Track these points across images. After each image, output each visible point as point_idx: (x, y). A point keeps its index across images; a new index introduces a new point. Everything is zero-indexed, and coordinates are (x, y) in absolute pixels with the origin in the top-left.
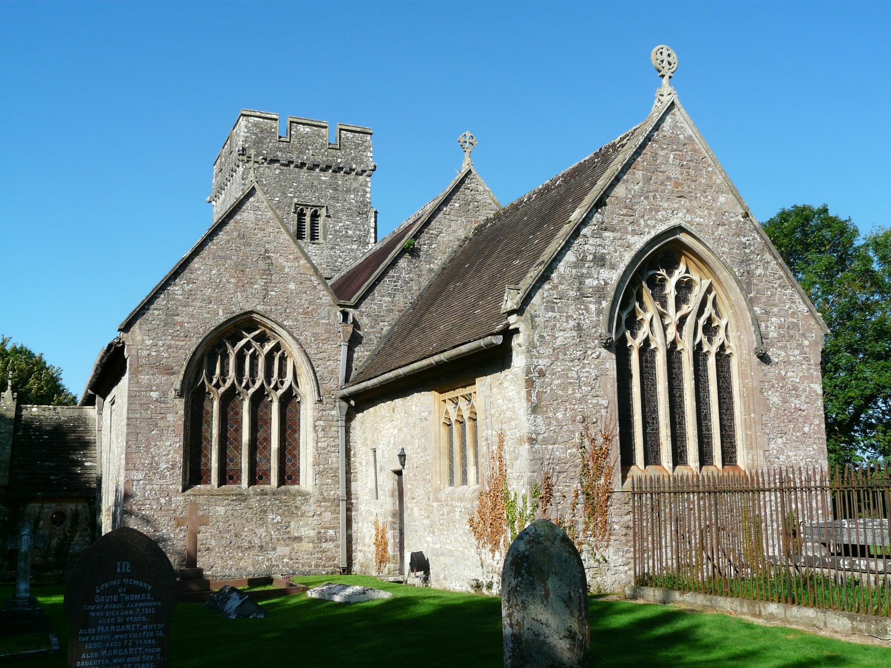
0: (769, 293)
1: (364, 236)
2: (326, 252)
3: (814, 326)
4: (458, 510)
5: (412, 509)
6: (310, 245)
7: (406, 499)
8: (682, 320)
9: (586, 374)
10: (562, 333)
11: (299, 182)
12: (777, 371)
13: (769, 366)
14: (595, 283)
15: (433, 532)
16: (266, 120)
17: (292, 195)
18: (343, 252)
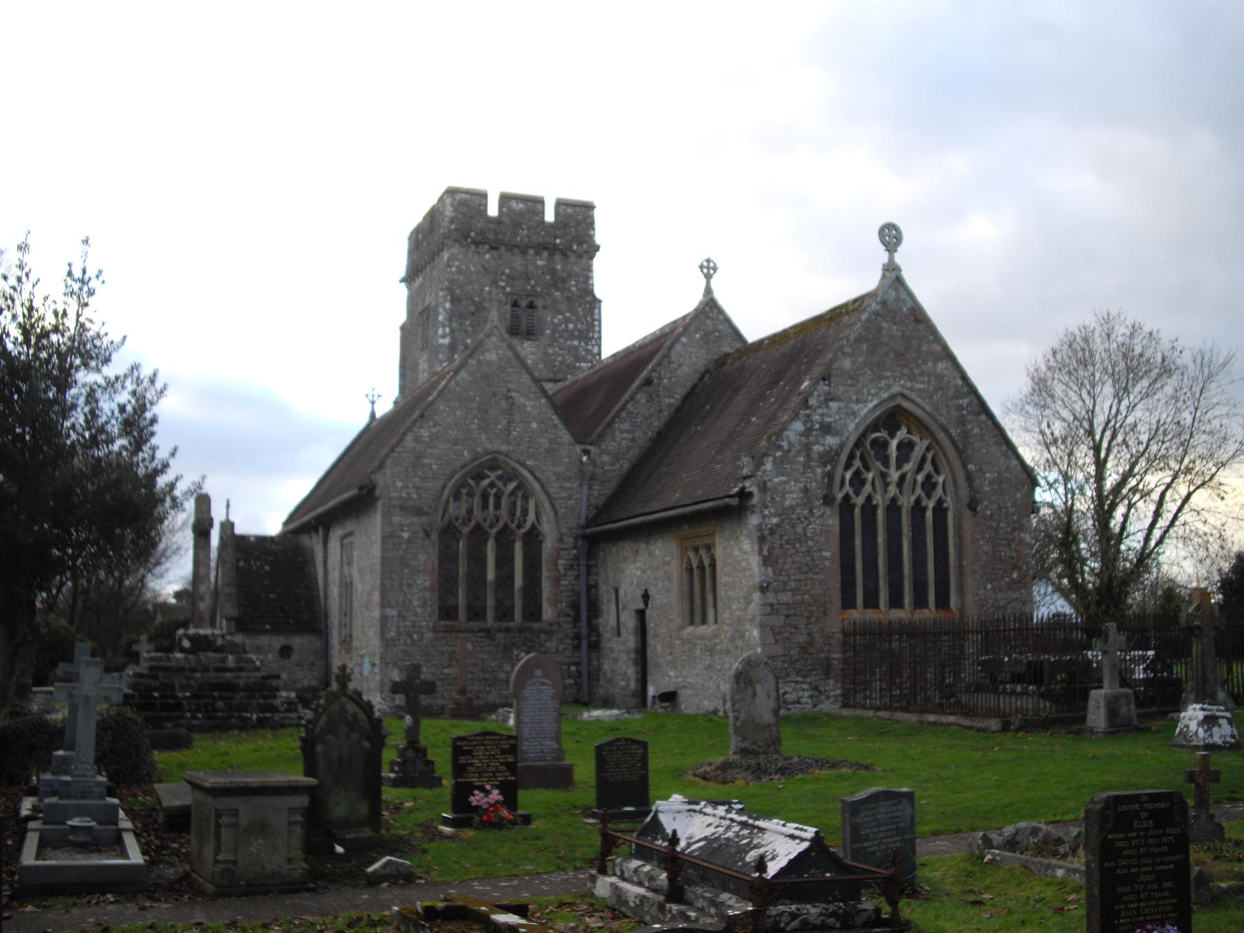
4: (698, 647)
5: (655, 646)
7: (650, 636)
8: (902, 478)
14: (821, 449)
15: (676, 668)
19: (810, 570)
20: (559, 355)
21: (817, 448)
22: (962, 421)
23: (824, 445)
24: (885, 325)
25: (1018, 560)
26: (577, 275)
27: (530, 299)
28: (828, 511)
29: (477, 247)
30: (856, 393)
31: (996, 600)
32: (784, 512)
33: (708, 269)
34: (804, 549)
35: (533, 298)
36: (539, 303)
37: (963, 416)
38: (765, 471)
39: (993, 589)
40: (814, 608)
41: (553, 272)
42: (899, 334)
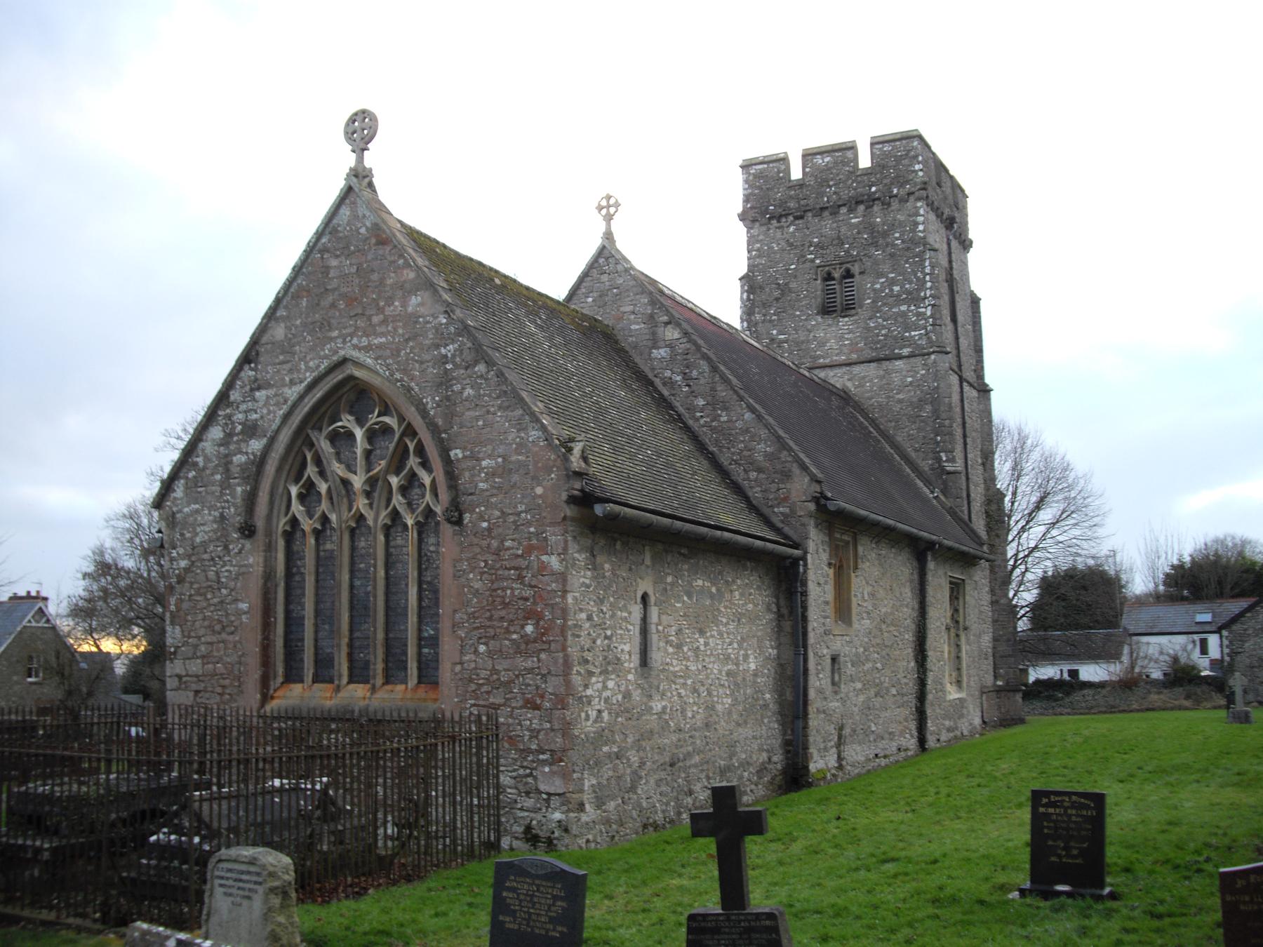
0: (480, 423)
9: (226, 574)
14: (243, 458)
19: (223, 628)
20: (884, 327)
21: (239, 459)
22: (445, 381)
23: (247, 453)
24: (334, 263)
25: (535, 603)
26: (901, 224)
27: (844, 266)
28: (248, 545)
29: (779, 221)
30: (291, 371)
31: (494, 671)
32: (194, 551)
33: (608, 209)
34: (216, 600)
35: (848, 265)
36: (856, 269)
37: (446, 370)
38: (175, 498)
39: (490, 653)
40: (227, 682)
41: (871, 228)
42: (354, 270)
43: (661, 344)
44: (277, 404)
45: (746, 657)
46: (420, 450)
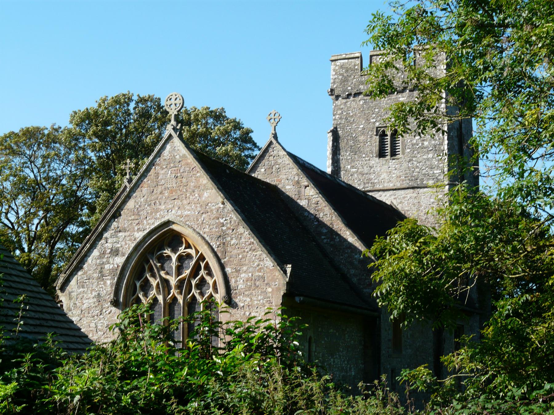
1: (439, 145)
2: (405, 165)
3: (278, 276)
6: (391, 161)
9: (101, 324)
10: (87, 301)
11: (380, 108)
12: (243, 313)
13: (236, 310)
14: (111, 266)
16: (350, 60)
17: (374, 120)
18: (420, 162)
43: (303, 197)
44: (130, 240)
45: (350, 369)
46: (207, 267)
